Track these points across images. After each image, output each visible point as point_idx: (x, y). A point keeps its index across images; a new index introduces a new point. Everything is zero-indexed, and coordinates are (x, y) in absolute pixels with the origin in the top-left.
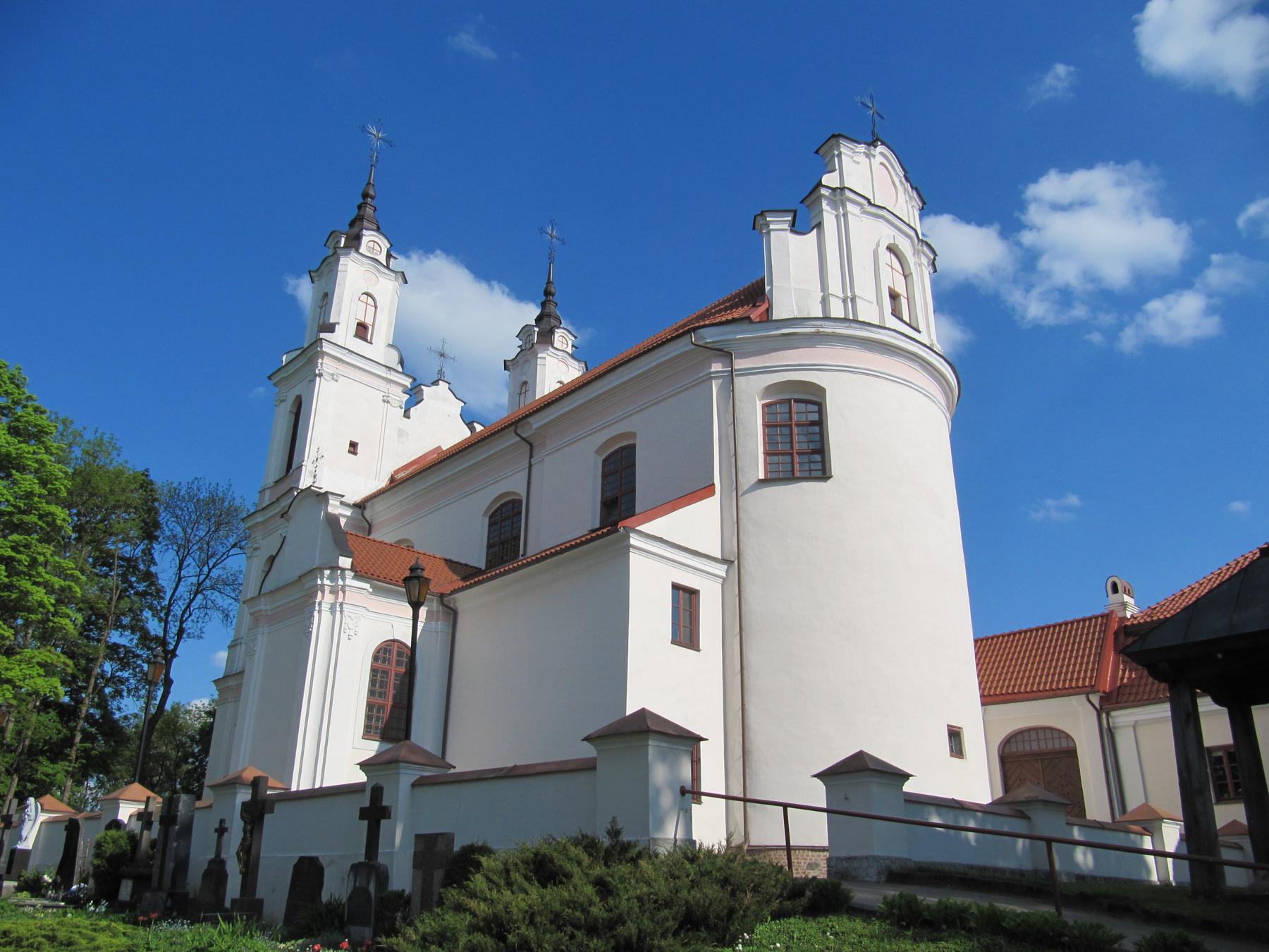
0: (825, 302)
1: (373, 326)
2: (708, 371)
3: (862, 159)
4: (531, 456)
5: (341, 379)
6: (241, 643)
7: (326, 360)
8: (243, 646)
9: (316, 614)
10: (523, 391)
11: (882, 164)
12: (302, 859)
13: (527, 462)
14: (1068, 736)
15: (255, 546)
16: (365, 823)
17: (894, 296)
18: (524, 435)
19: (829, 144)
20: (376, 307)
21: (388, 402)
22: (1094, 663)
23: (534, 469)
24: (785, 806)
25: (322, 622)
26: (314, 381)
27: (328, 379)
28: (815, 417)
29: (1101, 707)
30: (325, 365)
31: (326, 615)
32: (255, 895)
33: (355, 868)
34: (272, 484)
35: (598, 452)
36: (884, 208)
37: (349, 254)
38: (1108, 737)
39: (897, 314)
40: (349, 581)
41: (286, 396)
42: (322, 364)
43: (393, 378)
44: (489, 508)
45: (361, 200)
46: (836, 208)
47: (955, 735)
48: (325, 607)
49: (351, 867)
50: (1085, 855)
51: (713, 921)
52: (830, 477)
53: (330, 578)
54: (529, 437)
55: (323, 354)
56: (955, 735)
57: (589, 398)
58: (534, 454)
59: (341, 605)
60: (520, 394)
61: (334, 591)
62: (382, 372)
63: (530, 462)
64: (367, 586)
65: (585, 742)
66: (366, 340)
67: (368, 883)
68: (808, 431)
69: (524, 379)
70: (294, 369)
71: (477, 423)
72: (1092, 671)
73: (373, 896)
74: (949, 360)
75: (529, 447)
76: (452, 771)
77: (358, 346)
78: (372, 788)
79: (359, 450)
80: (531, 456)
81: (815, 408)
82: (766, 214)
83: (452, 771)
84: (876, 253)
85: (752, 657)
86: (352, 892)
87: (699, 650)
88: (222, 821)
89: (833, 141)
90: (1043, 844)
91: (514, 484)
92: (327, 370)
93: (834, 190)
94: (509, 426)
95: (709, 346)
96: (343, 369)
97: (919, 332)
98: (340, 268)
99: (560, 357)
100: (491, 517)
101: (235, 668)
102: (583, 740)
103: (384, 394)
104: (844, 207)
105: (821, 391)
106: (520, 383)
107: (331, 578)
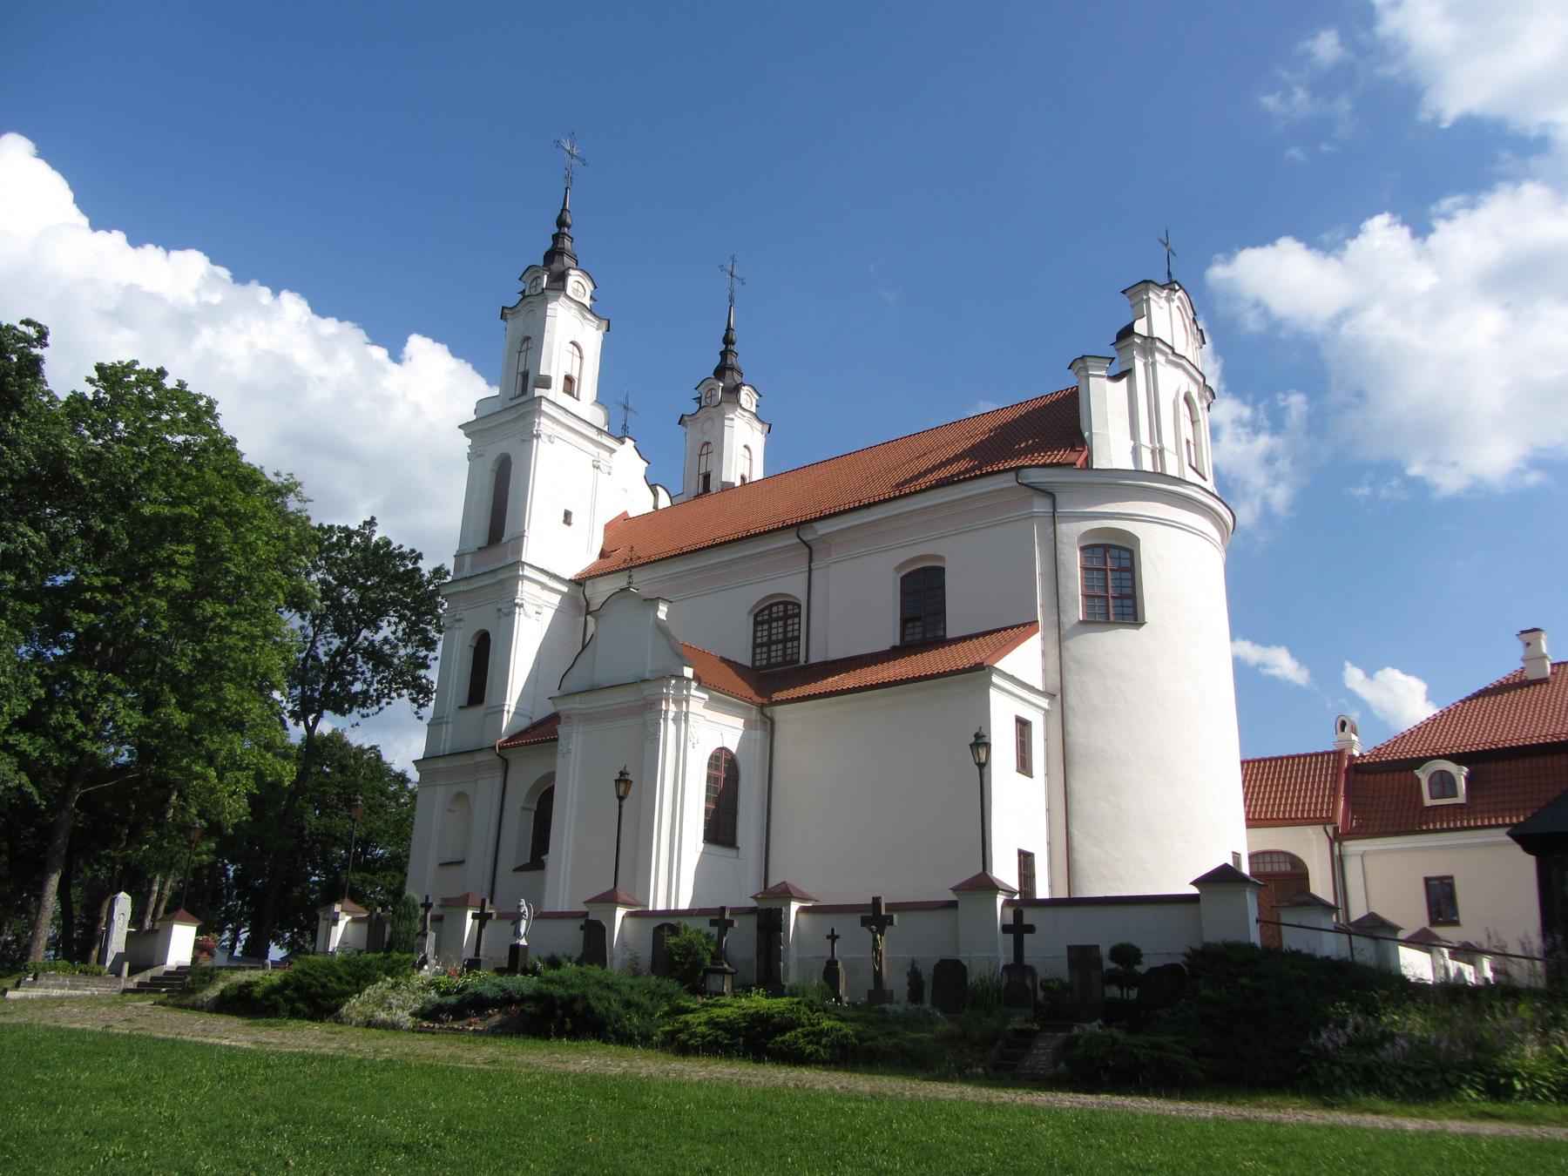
0: (1136, 453)
1: (579, 380)
3: (1163, 303)
4: (811, 561)
6: (447, 723)
7: (543, 420)
8: (450, 725)
9: (662, 721)
10: (704, 451)
11: (1178, 307)
15: (457, 617)
18: (804, 539)
19: (1139, 288)
20: (581, 358)
21: (598, 468)
22: (1329, 797)
23: (814, 573)
25: (669, 732)
26: (531, 441)
30: (544, 426)
31: (671, 727)
35: (898, 569)
36: (1184, 357)
37: (559, 297)
38: (1338, 865)
40: (693, 692)
42: (539, 424)
44: (755, 606)
45: (556, 230)
46: (1146, 357)
48: (671, 715)
50: (1536, 983)
52: (1143, 624)
53: (675, 687)
55: (542, 413)
57: (888, 514)
58: (814, 557)
59: (687, 714)
60: (701, 455)
61: (678, 702)
62: (593, 434)
63: (810, 567)
64: (706, 696)
66: (572, 395)
69: (706, 439)
70: (494, 424)
71: (661, 486)
72: (1328, 804)
75: (807, 550)
77: (565, 400)
79: (574, 519)
80: (811, 561)
82: (1090, 362)
85: (1077, 785)
87: (1032, 777)
89: (1143, 286)
91: (791, 584)
93: (1145, 337)
94: (792, 526)
97: (1205, 479)
98: (549, 312)
100: (756, 616)
104: (1153, 356)
106: (701, 443)
107: (676, 687)
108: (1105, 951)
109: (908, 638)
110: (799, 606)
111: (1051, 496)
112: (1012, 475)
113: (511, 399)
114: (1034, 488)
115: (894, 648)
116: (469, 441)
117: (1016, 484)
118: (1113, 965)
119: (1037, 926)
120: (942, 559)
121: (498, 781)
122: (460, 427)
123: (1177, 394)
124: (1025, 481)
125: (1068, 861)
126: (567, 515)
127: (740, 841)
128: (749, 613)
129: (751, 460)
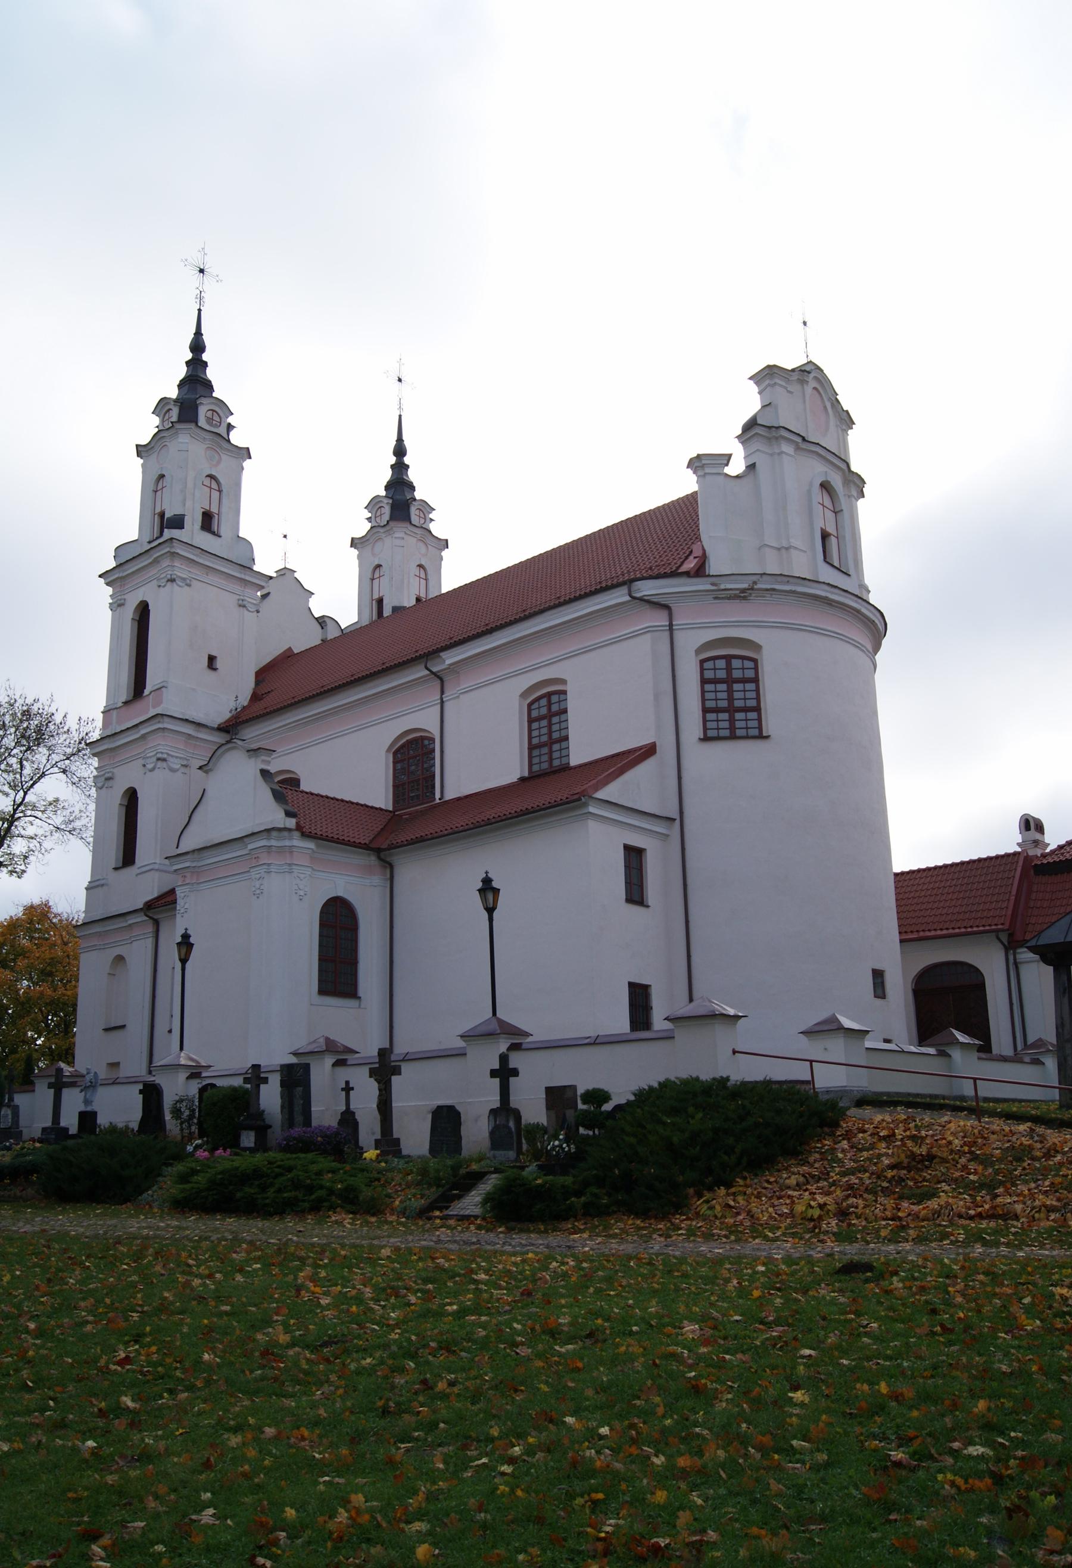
4: (442, 693)
5: (194, 583)
10: (377, 575)
11: (815, 388)
12: (440, 1108)
13: (439, 697)
14: (977, 970)
16: (497, 1080)
17: (825, 536)
18: (434, 670)
20: (220, 491)
21: (244, 606)
23: (447, 705)
24: (811, 1062)
27: (181, 584)
29: (1009, 943)
32: (392, 1135)
33: (493, 1112)
34: (120, 704)
35: (524, 695)
39: (828, 560)
41: (125, 600)
43: (247, 578)
47: (878, 975)
54: (439, 672)
56: (878, 975)
58: (446, 690)
63: (442, 699)
66: (213, 533)
67: (508, 1121)
73: (513, 1129)
77: (204, 540)
78: (500, 1056)
79: (219, 664)
80: (442, 693)
81: (751, 664)
84: (809, 492)
86: (493, 1128)
88: (347, 1083)
90: (972, 1081)
91: (426, 720)
92: (179, 574)
94: (421, 657)
95: (646, 598)
96: (196, 572)
99: (418, 536)
100: (395, 754)
103: (238, 597)
105: (757, 647)
108: (580, 1091)
109: (536, 768)
110: (433, 740)
111: (667, 607)
112: (624, 590)
113: (150, 542)
114: (648, 602)
115: (522, 780)
116: (110, 590)
117: (628, 598)
118: (585, 1107)
119: (520, 1071)
120: (563, 682)
121: (149, 942)
122: (100, 576)
123: (811, 484)
124: (638, 595)
125: (1021, 963)
126: (212, 659)
127: (361, 992)
128: (388, 750)
129: (426, 580)
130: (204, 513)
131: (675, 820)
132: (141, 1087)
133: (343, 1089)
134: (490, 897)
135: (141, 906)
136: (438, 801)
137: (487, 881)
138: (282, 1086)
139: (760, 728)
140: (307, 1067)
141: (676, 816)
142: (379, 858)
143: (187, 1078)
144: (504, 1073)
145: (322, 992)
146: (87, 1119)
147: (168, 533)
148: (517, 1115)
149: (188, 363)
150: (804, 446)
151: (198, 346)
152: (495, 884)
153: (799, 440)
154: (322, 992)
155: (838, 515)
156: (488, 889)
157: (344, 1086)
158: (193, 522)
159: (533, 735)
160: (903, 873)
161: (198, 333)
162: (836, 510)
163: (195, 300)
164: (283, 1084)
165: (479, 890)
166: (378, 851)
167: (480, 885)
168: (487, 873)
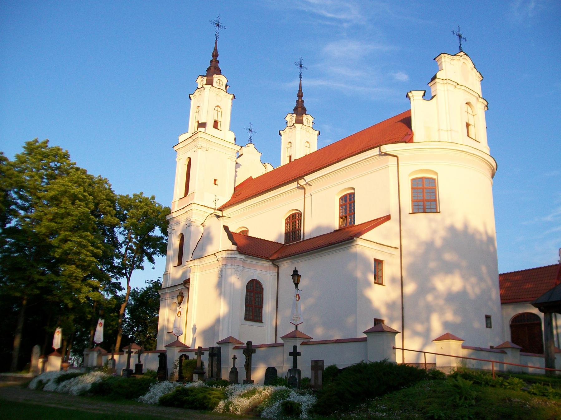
2: (387, 164)
17: (468, 125)
24: (214, 254)
28: (434, 198)
47: (488, 318)
49: (288, 370)
51: (364, 405)
65: (364, 334)
67: (295, 375)
68: (431, 207)
73: (297, 378)
74: (455, 355)
76: (312, 340)
83: (312, 340)
88: (235, 356)
101: (168, 284)
102: (363, 333)
126: (215, 180)
127: (263, 320)
130: (215, 121)
131: (398, 248)
132: (159, 354)
133: (233, 358)
134: (296, 278)
135: (183, 283)
136: (302, 240)
137: (295, 272)
138: (209, 356)
139: (436, 208)
140: (219, 349)
141: (399, 246)
142: (273, 264)
143: (179, 352)
144: (295, 354)
145: (246, 319)
146: (139, 367)
147: (200, 129)
148: (299, 372)
149: (211, 61)
150: (458, 86)
151: (215, 55)
152: (299, 273)
153: (456, 84)
154: (246, 319)
155: (474, 116)
156: (296, 275)
157: (233, 357)
158: (210, 125)
159: (341, 212)
160: (504, 274)
161: (216, 50)
162: (474, 114)
163: (214, 37)
164: (210, 355)
165: (292, 275)
166: (273, 261)
167: (292, 273)
168: (295, 268)
